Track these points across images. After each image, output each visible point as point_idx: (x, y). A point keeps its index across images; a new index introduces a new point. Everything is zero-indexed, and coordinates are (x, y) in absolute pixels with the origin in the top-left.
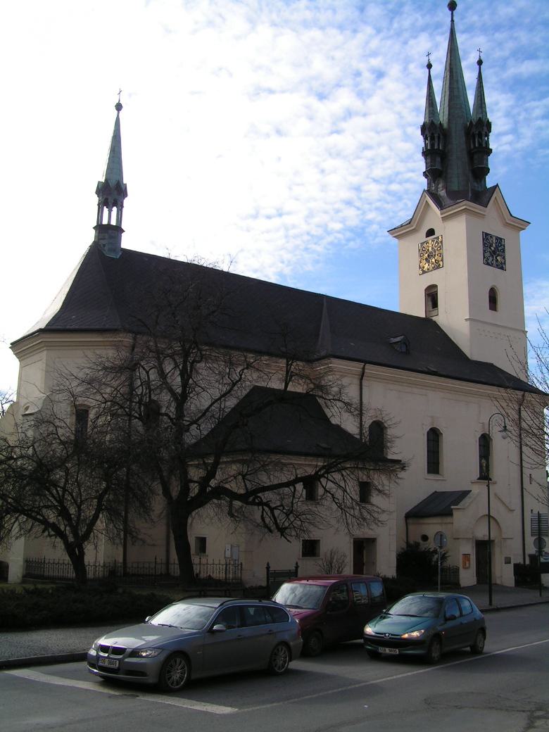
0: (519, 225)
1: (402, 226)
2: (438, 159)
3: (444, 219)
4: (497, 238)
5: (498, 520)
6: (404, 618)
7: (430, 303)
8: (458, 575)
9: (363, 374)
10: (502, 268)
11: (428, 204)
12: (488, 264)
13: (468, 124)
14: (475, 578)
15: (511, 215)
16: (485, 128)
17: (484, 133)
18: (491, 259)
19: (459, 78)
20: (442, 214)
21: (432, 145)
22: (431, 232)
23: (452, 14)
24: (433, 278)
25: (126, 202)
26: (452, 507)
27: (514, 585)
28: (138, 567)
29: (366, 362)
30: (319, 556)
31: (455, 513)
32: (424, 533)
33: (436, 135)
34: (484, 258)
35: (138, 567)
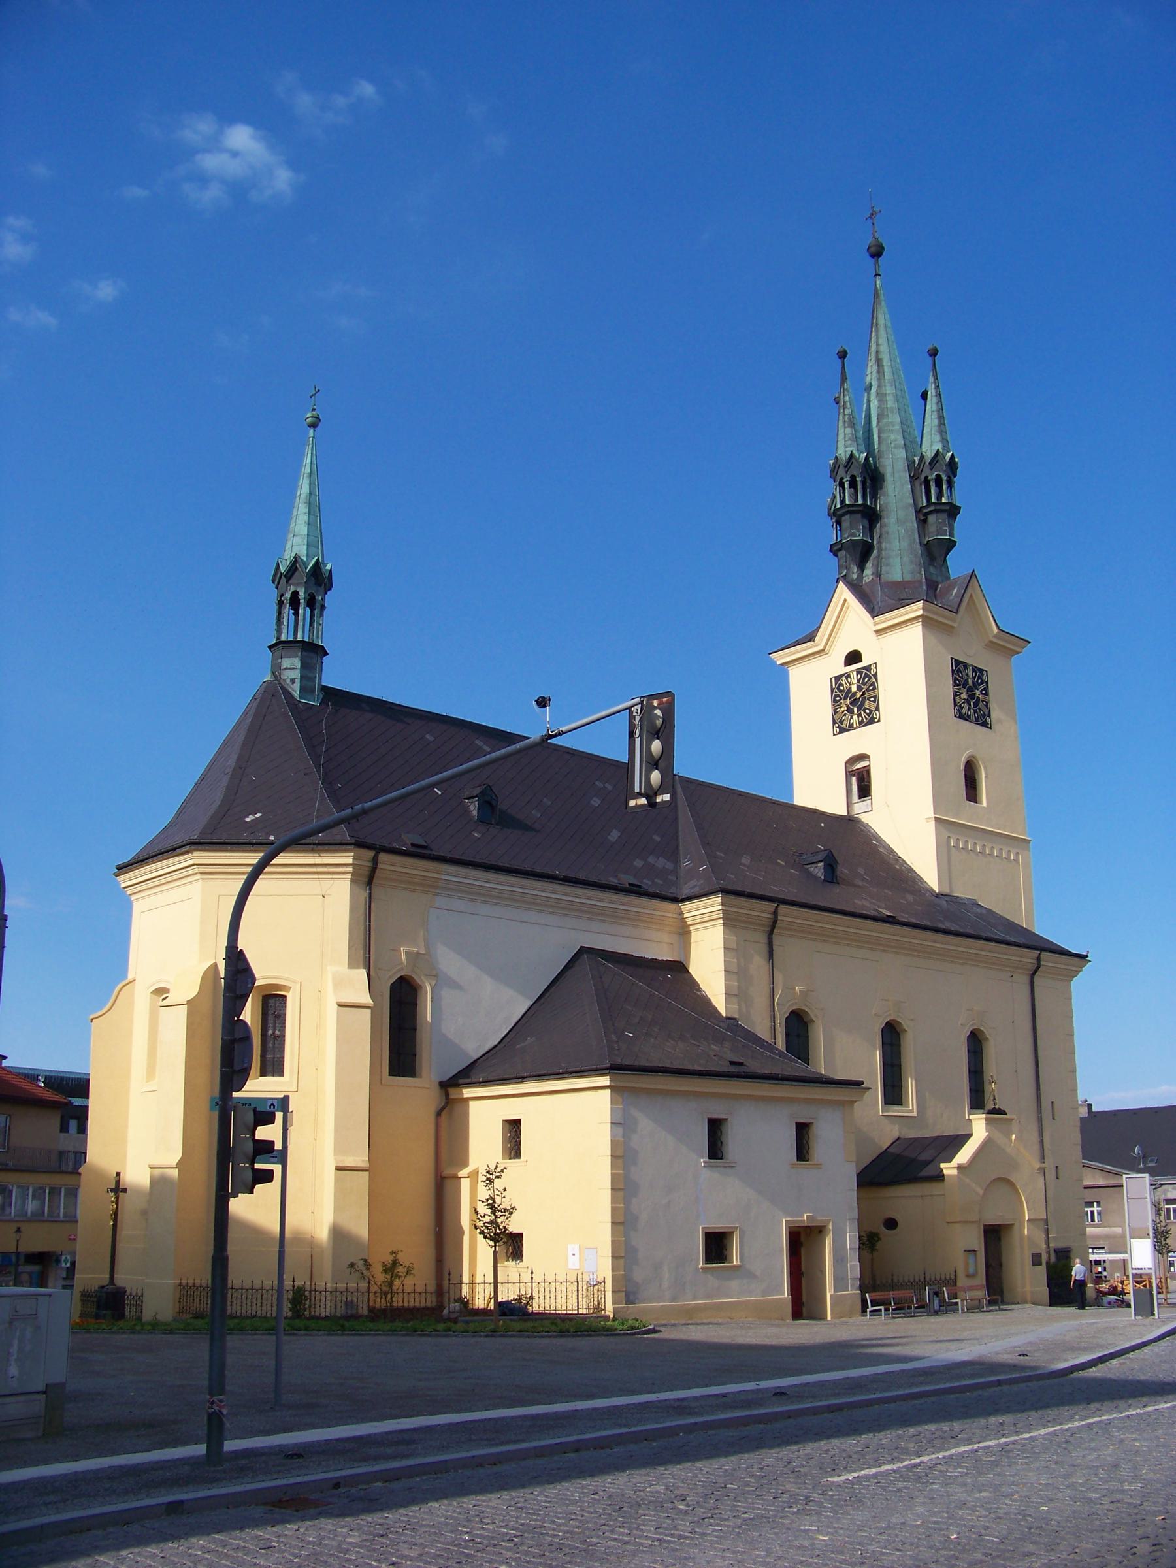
4: (975, 669)
6: (966, 1334)
9: (775, 922)
10: (984, 724)
12: (961, 717)
13: (917, 459)
18: (966, 707)
20: (875, 624)
22: (854, 657)
24: (859, 740)
29: (379, 849)
34: (955, 704)
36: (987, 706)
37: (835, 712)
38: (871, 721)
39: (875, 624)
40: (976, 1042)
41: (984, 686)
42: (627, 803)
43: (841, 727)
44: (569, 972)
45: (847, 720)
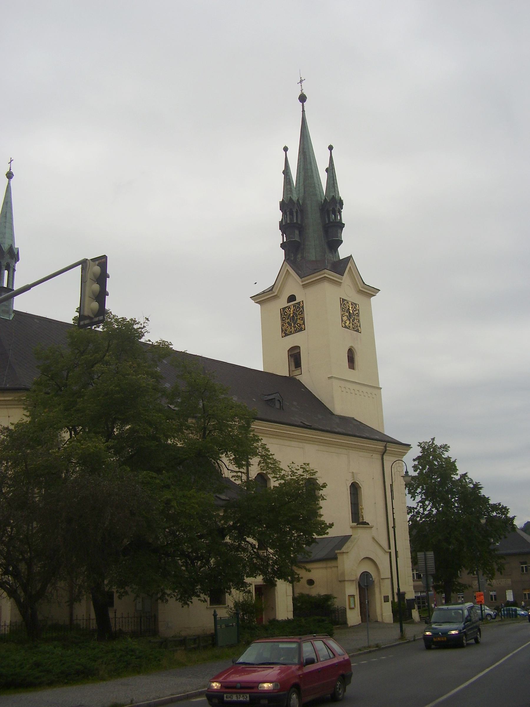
0: (370, 292)
1: (264, 292)
2: (297, 232)
3: (305, 286)
5: (377, 562)
7: (293, 364)
8: (346, 615)
10: (357, 331)
11: (289, 273)
12: (346, 327)
14: (360, 617)
15: (364, 283)
16: (338, 205)
17: (337, 209)
19: (312, 160)
21: (291, 220)
22: (292, 298)
23: (303, 105)
25: (18, 266)
26: (336, 551)
27: (392, 622)
28: (122, 617)
30: (224, 604)
31: (339, 557)
32: (309, 578)
33: (294, 210)
34: (342, 321)
35: (122, 617)
36: (359, 322)
37: (283, 325)
38: (301, 330)
39: (302, 282)
40: (355, 489)
41: (357, 312)
42: (289, 576)
43: (285, 333)
44: (30, 283)
45: (289, 329)
